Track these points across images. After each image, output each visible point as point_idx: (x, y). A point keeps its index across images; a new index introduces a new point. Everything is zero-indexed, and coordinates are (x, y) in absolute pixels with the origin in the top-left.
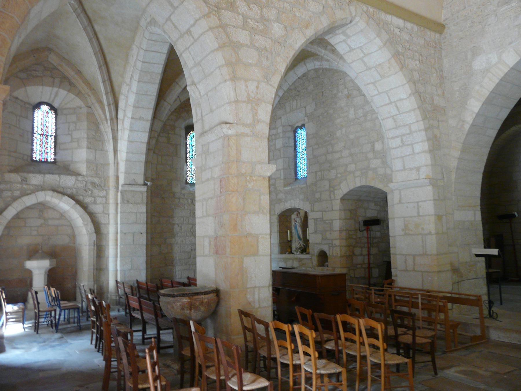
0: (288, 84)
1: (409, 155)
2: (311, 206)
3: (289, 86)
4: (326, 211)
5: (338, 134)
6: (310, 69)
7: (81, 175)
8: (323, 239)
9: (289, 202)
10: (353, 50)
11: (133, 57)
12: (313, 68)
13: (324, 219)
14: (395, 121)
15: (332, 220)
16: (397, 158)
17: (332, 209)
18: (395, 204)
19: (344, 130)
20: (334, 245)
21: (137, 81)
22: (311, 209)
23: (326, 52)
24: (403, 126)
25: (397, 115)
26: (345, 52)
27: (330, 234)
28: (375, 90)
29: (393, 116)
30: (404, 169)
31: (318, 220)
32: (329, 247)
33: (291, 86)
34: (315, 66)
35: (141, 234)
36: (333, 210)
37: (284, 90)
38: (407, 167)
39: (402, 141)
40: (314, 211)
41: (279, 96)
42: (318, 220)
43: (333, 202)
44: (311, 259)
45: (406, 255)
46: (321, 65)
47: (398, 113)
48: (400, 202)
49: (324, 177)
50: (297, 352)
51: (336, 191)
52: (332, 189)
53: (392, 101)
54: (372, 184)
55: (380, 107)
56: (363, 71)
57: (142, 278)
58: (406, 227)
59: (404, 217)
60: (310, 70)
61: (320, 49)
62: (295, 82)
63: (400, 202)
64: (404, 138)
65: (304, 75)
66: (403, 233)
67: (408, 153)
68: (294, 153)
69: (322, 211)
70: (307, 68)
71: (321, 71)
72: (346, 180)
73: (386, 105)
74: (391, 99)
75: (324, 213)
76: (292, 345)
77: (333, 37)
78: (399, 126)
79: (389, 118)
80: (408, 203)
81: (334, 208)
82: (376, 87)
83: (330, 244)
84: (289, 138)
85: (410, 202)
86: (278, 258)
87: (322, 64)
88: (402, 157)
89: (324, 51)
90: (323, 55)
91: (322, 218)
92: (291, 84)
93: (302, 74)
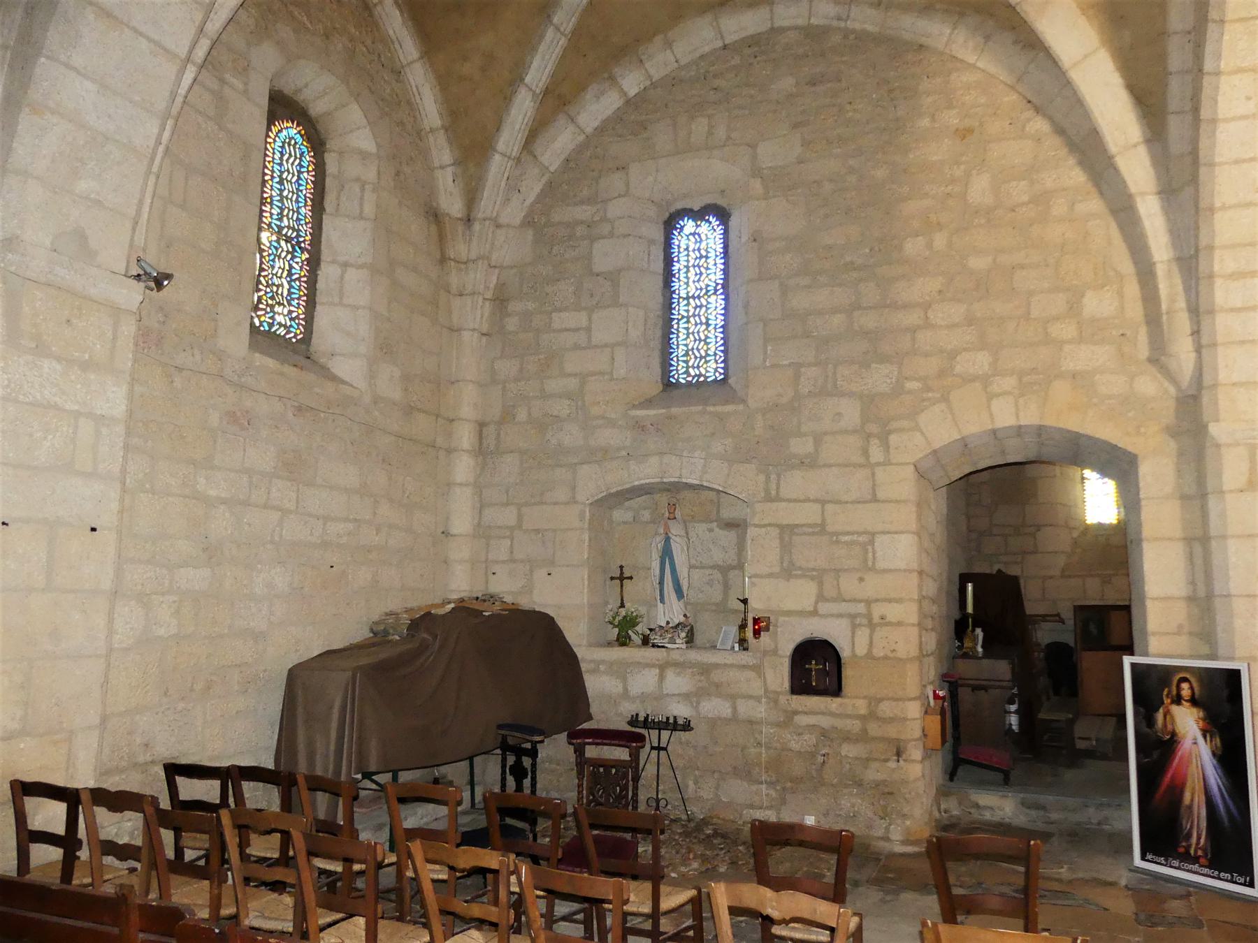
5: (913, 247)
9: (654, 460)
17: (874, 494)
18: (1231, 491)
19: (940, 240)
20: (876, 619)
22: (767, 491)
27: (861, 579)
32: (854, 627)
33: (681, 68)
35: (93, 526)
36: (875, 499)
37: (650, 77)
43: (880, 472)
46: (839, 19)
49: (835, 385)
50: (445, 936)
60: (782, 30)
61: (354, 113)
65: (753, 42)
68: (664, 295)
69: (823, 502)
72: (945, 399)
76: (255, 859)
81: (881, 495)
84: (652, 242)
91: (823, 525)
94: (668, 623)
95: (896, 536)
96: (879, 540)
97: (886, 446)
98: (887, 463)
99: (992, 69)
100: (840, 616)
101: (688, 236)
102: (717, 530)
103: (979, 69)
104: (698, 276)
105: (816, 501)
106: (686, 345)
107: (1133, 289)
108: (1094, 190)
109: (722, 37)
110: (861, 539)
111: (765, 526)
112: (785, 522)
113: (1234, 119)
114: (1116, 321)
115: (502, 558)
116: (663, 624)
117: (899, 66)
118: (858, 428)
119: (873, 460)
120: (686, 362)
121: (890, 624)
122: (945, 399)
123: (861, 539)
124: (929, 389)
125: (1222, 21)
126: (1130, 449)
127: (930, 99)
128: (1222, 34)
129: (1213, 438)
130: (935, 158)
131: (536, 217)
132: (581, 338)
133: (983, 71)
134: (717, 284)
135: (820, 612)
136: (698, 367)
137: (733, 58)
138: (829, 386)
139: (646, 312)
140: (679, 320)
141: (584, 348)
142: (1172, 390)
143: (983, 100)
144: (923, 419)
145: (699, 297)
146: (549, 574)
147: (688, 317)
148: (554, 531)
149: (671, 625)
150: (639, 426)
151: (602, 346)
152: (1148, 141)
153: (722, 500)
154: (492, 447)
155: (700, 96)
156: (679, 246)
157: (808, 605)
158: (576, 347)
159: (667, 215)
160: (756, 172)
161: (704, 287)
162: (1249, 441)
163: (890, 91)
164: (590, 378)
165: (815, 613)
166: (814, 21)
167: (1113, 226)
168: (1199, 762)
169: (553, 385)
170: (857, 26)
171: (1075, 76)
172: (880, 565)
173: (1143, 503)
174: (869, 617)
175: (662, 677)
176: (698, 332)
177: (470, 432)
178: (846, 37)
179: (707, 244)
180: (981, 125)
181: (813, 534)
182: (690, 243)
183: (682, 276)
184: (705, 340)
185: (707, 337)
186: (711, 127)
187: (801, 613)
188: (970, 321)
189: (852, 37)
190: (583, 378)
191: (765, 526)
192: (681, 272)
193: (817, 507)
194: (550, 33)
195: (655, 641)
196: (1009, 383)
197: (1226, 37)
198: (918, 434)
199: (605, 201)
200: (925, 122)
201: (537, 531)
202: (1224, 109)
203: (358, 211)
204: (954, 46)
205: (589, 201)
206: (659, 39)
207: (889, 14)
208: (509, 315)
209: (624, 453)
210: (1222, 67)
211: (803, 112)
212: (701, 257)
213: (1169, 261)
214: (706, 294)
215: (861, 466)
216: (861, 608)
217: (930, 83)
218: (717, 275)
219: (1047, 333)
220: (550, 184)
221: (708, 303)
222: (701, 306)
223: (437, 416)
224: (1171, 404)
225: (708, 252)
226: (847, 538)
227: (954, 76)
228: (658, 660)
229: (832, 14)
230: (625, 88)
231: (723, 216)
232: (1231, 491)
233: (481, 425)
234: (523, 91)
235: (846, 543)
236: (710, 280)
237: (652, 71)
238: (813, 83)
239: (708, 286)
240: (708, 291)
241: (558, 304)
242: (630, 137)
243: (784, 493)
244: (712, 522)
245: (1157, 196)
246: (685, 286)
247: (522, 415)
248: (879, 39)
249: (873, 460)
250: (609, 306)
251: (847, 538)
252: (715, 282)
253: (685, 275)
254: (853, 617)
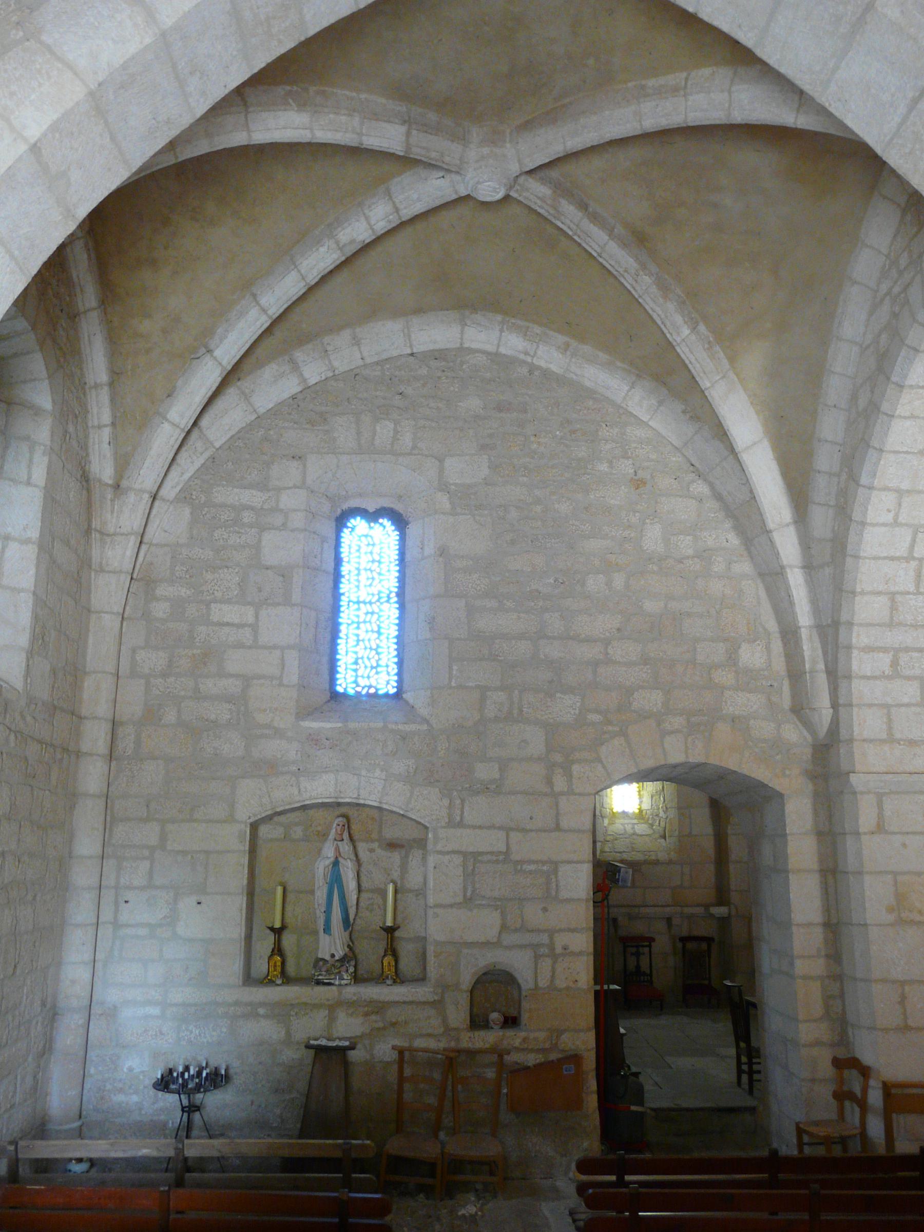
0: (359, 356)
1: (908, 705)
2: (451, 806)
4: (524, 831)
6: (474, 346)
7: (577, 430)
8: (504, 927)
12: (491, 348)
13: (515, 857)
14: (893, 608)
15: (555, 865)
16: (870, 706)
17: (558, 825)
18: (865, 834)
19: (619, 581)
20: (559, 950)
22: (450, 816)
23: (693, 337)
24: (912, 626)
25: (908, 593)
27: (545, 910)
28: (889, 511)
29: (894, 594)
30: (891, 740)
31: (486, 858)
32: (537, 957)
33: (365, 366)
36: (558, 828)
38: (898, 736)
39: (895, 663)
40: (461, 824)
42: (486, 858)
43: (563, 801)
44: (438, 1005)
45: (903, 983)
46: (526, 353)
47: (912, 589)
48: (880, 828)
51: (576, 768)
52: (558, 758)
53: (916, 555)
54: (731, 763)
55: (869, 558)
57: (780, 1154)
58: (901, 898)
59: (895, 874)
60: (471, 351)
61: (679, 319)
63: (880, 828)
64: (904, 658)
65: (438, 355)
66: (891, 918)
67: (906, 700)
69: (508, 830)
70: (462, 339)
71: (524, 370)
72: (623, 734)
73: (892, 559)
74: (916, 549)
75: (515, 837)
78: (900, 624)
79: (879, 593)
80: (908, 833)
81: (564, 824)
82: (900, 505)
83: (539, 945)
85: (914, 833)
86: (237, 1003)
88: (887, 706)
89: (686, 331)
90: (679, 340)
91: (507, 853)
92: (368, 360)
94: (333, 956)
95: (578, 865)
96: (563, 869)
97: (569, 775)
98: (570, 792)
99: (663, 432)
100: (522, 947)
101: (360, 537)
102: (379, 851)
103: (651, 427)
104: (370, 581)
105: (500, 828)
106: (356, 653)
107: (777, 646)
108: (745, 553)
109: (411, 346)
110: (545, 868)
111: (448, 853)
112: (471, 849)
113: (877, 525)
114: (766, 673)
115: (136, 883)
116: (327, 957)
117: (580, 410)
118: (543, 756)
119: (557, 789)
120: (356, 670)
121: (573, 954)
122: (623, 734)
123: (545, 868)
124: (610, 723)
125: (881, 449)
126: (777, 788)
127: (608, 446)
128: (880, 460)
129: (852, 786)
130: (612, 502)
131: (194, 493)
132: (246, 635)
133: (654, 429)
134: (391, 592)
135: (505, 943)
136: (368, 677)
137: (420, 367)
138: (515, 712)
139: (317, 614)
140: (348, 624)
141: (250, 647)
142: (809, 738)
143: (654, 456)
144: (603, 750)
145: (370, 603)
146: (199, 903)
147: (358, 623)
148: (207, 853)
149: (337, 958)
150: (314, 739)
151: (270, 648)
152: (795, 522)
153: (384, 818)
154: (129, 752)
155: (385, 398)
156: (350, 547)
157: (491, 934)
158: (240, 645)
159: (339, 512)
160: (443, 487)
161: (376, 593)
162: (877, 790)
163: (573, 432)
164: (255, 681)
165: (498, 944)
166: (503, 350)
167: (761, 588)
168: (18, 946)
169: (210, 686)
170: (542, 364)
171: (745, 457)
172: (564, 894)
173: (789, 838)
174: (552, 947)
175: (332, 1019)
176: (369, 640)
177: (107, 734)
178: (531, 372)
179: (381, 549)
180: (652, 477)
181: (497, 862)
182: (362, 545)
183: (353, 578)
184: (376, 650)
185: (378, 646)
186: (396, 432)
187: (487, 944)
188: (645, 660)
189: (537, 373)
190: (247, 680)
191: (448, 853)
192: (352, 574)
193: (501, 835)
194: (254, 313)
195: (320, 977)
196: (678, 722)
197: (882, 462)
198: (600, 765)
199: (279, 490)
200: (604, 467)
201: (184, 853)
202: (871, 516)
203: (26, 478)
204: (630, 402)
205: (263, 486)
206: (346, 334)
207: (573, 360)
208: (158, 600)
209: (294, 768)
210: (875, 484)
211: (491, 436)
212: (373, 561)
213: (810, 627)
214: (378, 601)
215: (546, 795)
216: (545, 938)
217: (608, 431)
218: (392, 583)
219: (710, 678)
220: (213, 458)
221: (380, 610)
222: (373, 613)
223: (73, 714)
224: (808, 751)
225: (381, 557)
226: (532, 867)
227: (629, 430)
228: (328, 1000)
229: (520, 348)
230: (307, 374)
231: (400, 522)
232: (865, 834)
233: (114, 724)
234: (210, 363)
235: (531, 872)
236: (383, 586)
237: (336, 364)
238: (499, 408)
239: (379, 592)
240: (380, 598)
241: (219, 595)
242: (307, 426)
243: (468, 818)
244: (373, 841)
245: (802, 571)
246: (356, 589)
247: (170, 716)
248: (561, 380)
249: (557, 789)
250: (279, 604)
251: (532, 867)
252: (388, 589)
253: (356, 578)
254: (535, 947)
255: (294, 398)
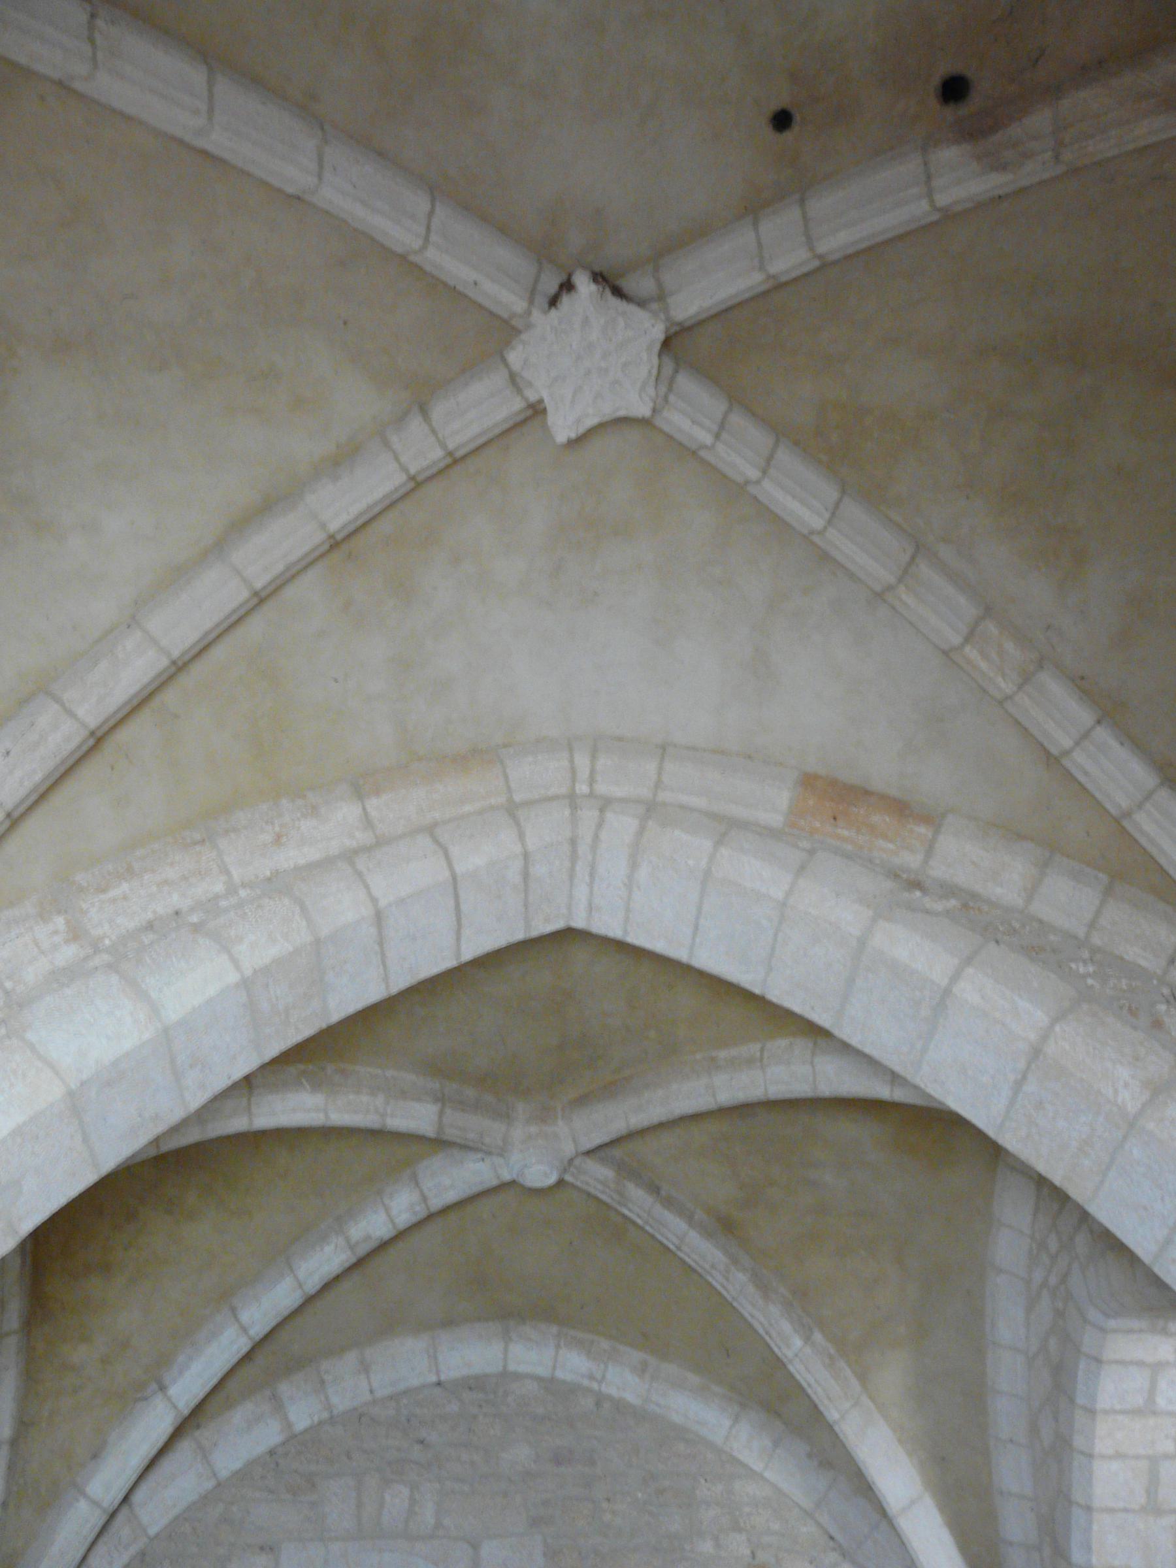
3: (367, 1397)
6: (522, 1369)
10: (1154, 1413)
11: (278, 839)
12: (541, 1371)
21: (248, 972)
23: (808, 1350)
26: (1118, 1407)
34: (554, 1368)
37: (329, 1407)
41: (289, 1425)
46: (591, 1377)
56: (1126, 1510)
60: (517, 1376)
61: (786, 1326)
62: (406, 1392)
65: (475, 1383)
77: (1141, 1331)
87: (604, 1377)
89: (798, 1342)
92: (379, 1394)
93: (465, 1372)
230: (292, 1417)
255: (272, 1452)
